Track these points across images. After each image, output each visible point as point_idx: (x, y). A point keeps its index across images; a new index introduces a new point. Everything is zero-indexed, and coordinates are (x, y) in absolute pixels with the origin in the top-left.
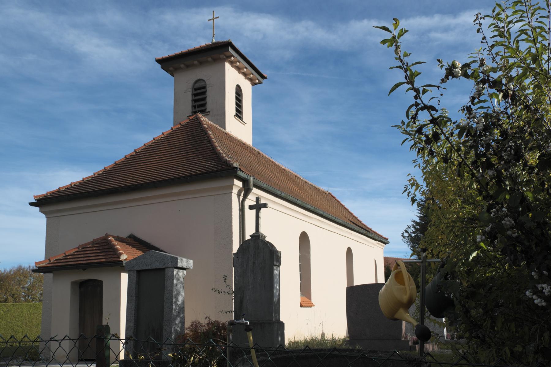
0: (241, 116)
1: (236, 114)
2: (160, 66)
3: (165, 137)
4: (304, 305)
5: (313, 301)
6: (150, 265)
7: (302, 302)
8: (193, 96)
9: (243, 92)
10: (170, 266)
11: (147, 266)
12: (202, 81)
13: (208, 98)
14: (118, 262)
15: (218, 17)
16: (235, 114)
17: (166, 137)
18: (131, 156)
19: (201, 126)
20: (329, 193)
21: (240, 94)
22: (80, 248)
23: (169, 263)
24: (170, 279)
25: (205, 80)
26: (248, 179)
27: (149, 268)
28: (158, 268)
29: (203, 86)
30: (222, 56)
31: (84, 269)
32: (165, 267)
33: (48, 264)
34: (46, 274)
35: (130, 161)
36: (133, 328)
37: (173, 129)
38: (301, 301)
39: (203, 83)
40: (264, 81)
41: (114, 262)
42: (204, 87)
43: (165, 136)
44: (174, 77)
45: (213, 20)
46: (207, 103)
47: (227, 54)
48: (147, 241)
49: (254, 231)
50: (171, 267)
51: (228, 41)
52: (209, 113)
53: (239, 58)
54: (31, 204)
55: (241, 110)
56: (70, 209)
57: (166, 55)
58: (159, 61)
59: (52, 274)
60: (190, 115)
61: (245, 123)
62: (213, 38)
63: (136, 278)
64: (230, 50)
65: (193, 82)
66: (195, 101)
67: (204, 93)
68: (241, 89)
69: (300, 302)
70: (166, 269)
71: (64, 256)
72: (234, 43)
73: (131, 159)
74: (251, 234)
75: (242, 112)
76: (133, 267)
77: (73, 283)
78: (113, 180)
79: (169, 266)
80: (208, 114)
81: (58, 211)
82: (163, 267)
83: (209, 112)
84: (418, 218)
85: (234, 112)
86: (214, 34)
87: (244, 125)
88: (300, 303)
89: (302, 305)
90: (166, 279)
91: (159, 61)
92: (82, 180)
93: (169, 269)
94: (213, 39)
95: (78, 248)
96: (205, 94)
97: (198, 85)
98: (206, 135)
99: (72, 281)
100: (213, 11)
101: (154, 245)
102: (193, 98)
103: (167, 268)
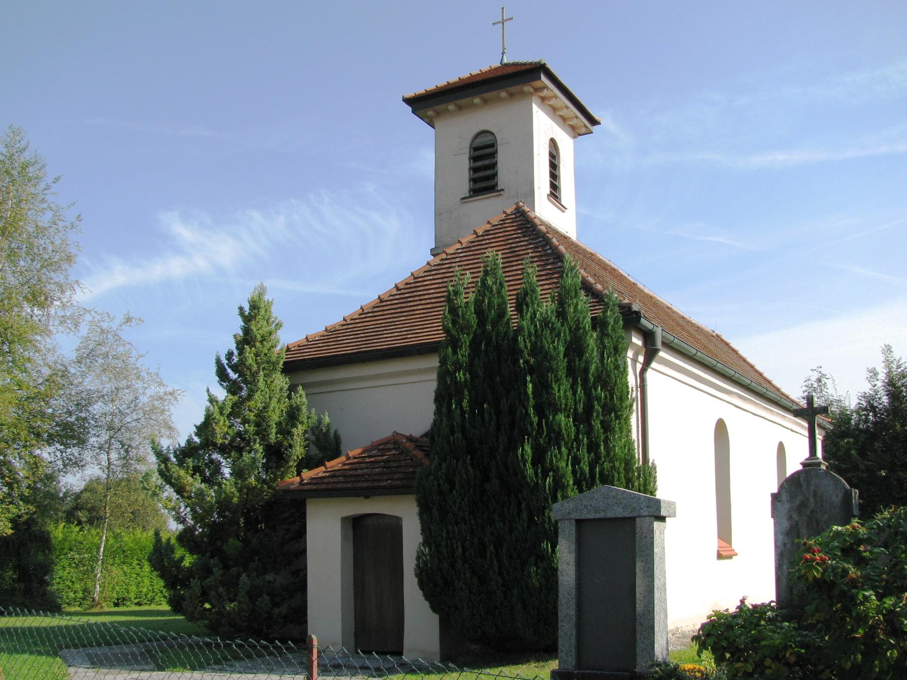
0: (557, 195)
1: (551, 191)
2: (410, 109)
3: (463, 248)
4: (723, 553)
5: (734, 546)
6: (604, 511)
7: (720, 549)
8: (472, 161)
9: (561, 152)
10: (646, 513)
11: (596, 512)
12: (489, 134)
16: (549, 193)
17: (467, 248)
18: (407, 284)
19: (532, 227)
20: (717, 336)
21: (555, 154)
23: (642, 509)
24: (646, 537)
25: (495, 132)
26: (654, 330)
27: (602, 515)
28: (620, 516)
29: (490, 143)
30: (527, 88)
32: (635, 515)
35: (407, 295)
36: (574, 618)
38: (718, 547)
39: (491, 137)
40: (595, 128)
42: (493, 145)
43: (464, 246)
44: (434, 128)
45: (503, 23)
46: (498, 173)
47: (537, 84)
49: (807, 455)
50: (646, 516)
52: (502, 192)
53: (557, 92)
55: (557, 184)
57: (420, 90)
58: (409, 101)
60: (466, 196)
61: (565, 208)
63: (576, 532)
64: (543, 77)
66: (474, 170)
67: (493, 155)
69: (717, 548)
70: (638, 519)
73: (410, 290)
74: (802, 459)
75: (560, 189)
76: (569, 513)
77: (344, 520)
78: (385, 332)
79: (644, 514)
80: (501, 195)
82: (631, 515)
83: (502, 190)
85: (547, 189)
86: (504, 49)
87: (563, 212)
88: (718, 551)
89: (722, 555)
90: (637, 535)
91: (409, 101)
92: (325, 331)
93: (642, 519)
96: (494, 157)
97: (480, 141)
98: (547, 245)
99: (346, 515)
100: (503, 8)
102: (471, 164)
103: (639, 516)
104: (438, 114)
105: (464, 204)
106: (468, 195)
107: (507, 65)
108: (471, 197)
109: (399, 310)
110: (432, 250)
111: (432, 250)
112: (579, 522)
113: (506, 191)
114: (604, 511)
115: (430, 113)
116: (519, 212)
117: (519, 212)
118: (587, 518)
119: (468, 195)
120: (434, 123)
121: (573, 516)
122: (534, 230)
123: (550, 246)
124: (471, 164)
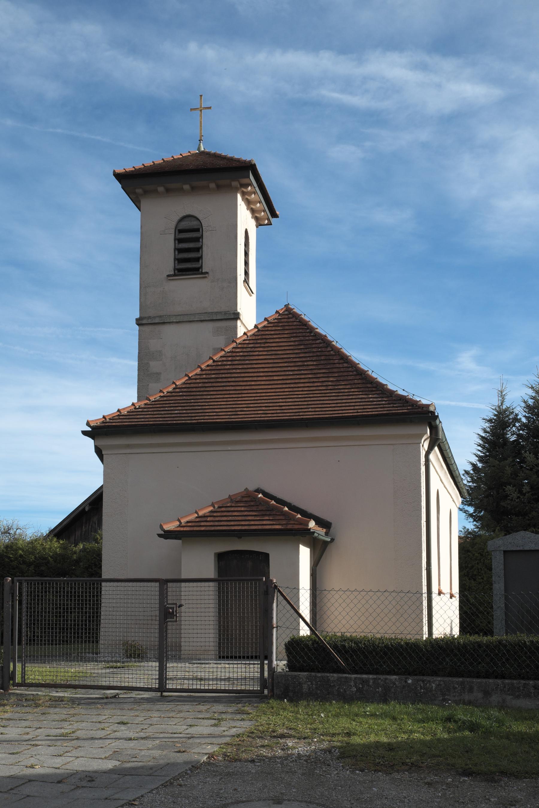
6: (522, 546)
8: (177, 242)
13: (204, 248)
14: (305, 530)
15: (210, 108)
22: (216, 506)
27: (521, 548)
28: (532, 549)
29: (196, 227)
30: (235, 184)
31: (240, 537)
33: (177, 527)
34: (168, 540)
37: (259, 327)
40: (273, 220)
41: (298, 530)
45: (201, 111)
47: (245, 181)
48: (286, 500)
51: (250, 161)
52: (207, 275)
54: (85, 433)
56: (151, 446)
57: (129, 168)
58: (119, 177)
59: (180, 541)
62: (200, 142)
65: (178, 218)
68: (248, 238)
71: (197, 517)
72: (260, 169)
77: (215, 554)
80: (206, 277)
81: (128, 446)
83: (207, 273)
84: (477, 458)
87: (251, 296)
94: (200, 145)
95: (213, 505)
97: (185, 225)
100: (201, 96)
101: (297, 506)
102: (177, 245)
104: (146, 193)
105: (169, 281)
106: (172, 273)
107: (203, 153)
108: (175, 275)
109: (320, 406)
110: (137, 320)
111: (137, 320)
112: (505, 552)
113: (210, 273)
114: (522, 546)
115: (139, 191)
116: (290, 314)
117: (290, 314)
118: (512, 550)
119: (172, 273)
120: (140, 202)
121: (502, 548)
122: (311, 332)
123: (331, 348)
124: (177, 245)
